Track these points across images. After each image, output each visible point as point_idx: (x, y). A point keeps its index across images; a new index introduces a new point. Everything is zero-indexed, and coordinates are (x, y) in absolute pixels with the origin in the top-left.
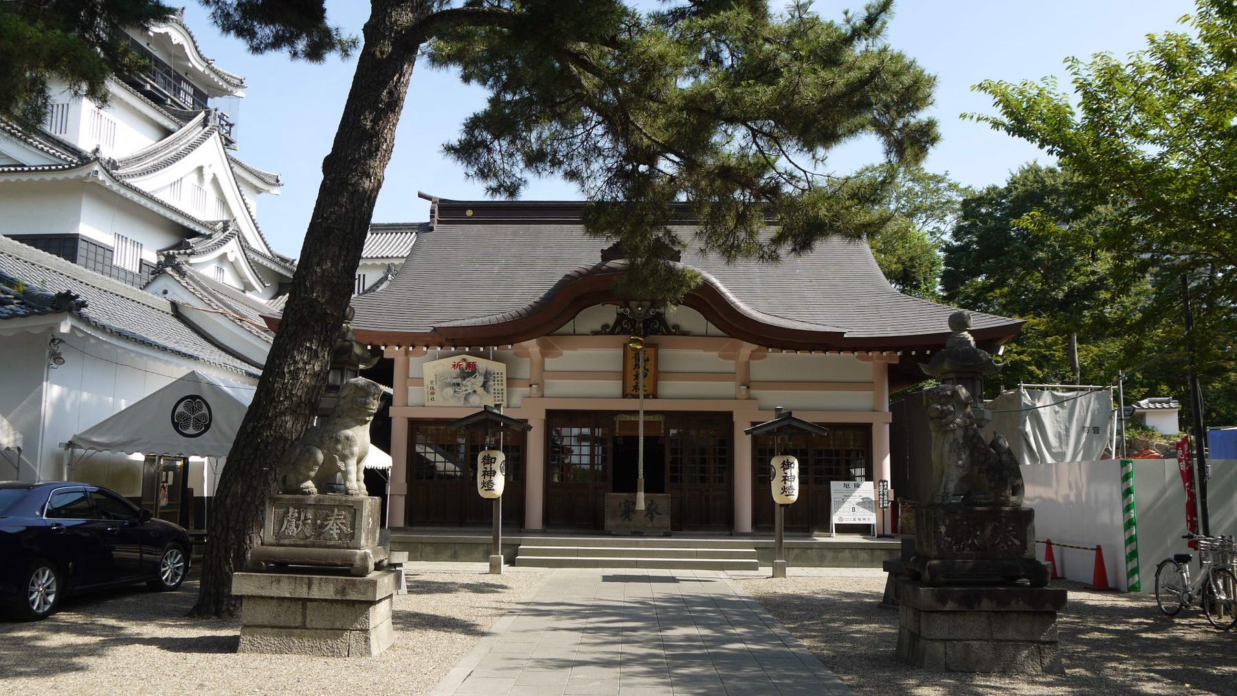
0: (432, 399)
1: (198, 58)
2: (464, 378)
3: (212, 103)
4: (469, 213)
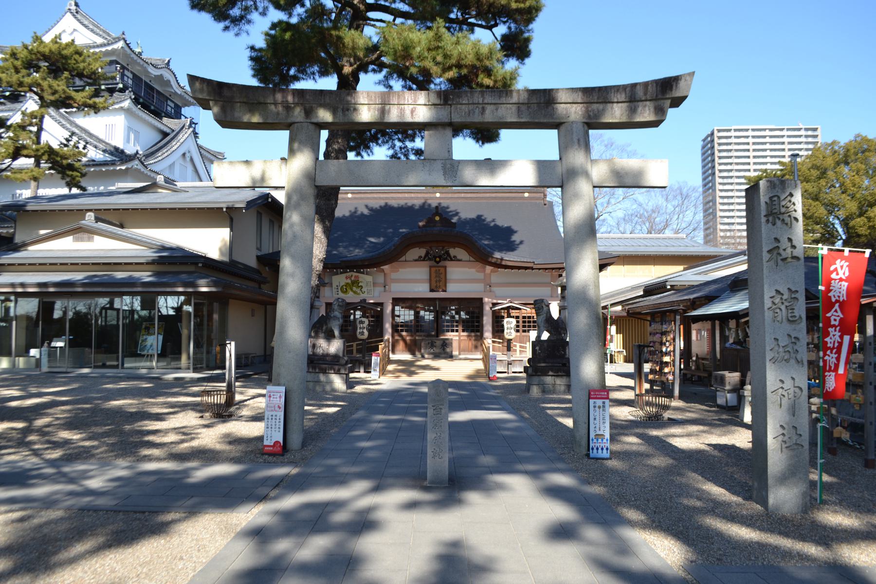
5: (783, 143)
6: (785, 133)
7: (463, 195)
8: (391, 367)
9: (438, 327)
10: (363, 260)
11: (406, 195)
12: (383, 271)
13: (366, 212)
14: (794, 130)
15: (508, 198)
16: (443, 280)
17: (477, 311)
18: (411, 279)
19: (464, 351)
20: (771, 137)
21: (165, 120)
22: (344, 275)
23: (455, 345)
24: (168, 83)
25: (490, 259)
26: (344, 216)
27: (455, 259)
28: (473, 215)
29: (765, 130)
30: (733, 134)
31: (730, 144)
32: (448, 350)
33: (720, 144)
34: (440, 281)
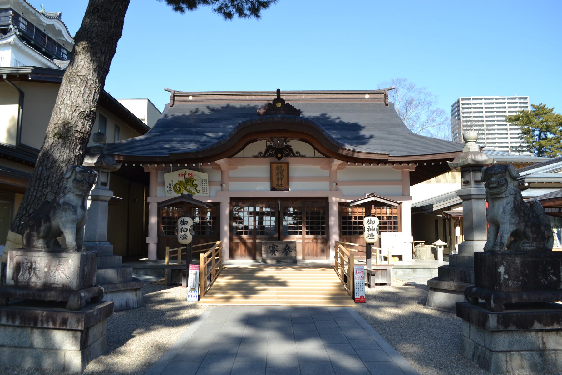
5: (505, 107)
6: (506, 101)
7: (304, 97)
8: (222, 281)
9: (280, 232)
10: (195, 152)
11: (247, 97)
12: (219, 168)
13: (207, 111)
14: (512, 98)
15: (349, 99)
16: (285, 177)
17: (321, 211)
18: (250, 177)
19: (309, 255)
20: (497, 103)
21: (56, 61)
22: (177, 173)
23: (299, 248)
24: (59, 33)
25: (340, 151)
26: (184, 115)
27: (298, 155)
28: (317, 114)
29: (493, 99)
30: (471, 101)
31: (470, 108)
32: (293, 254)
33: (463, 108)
34: (282, 179)
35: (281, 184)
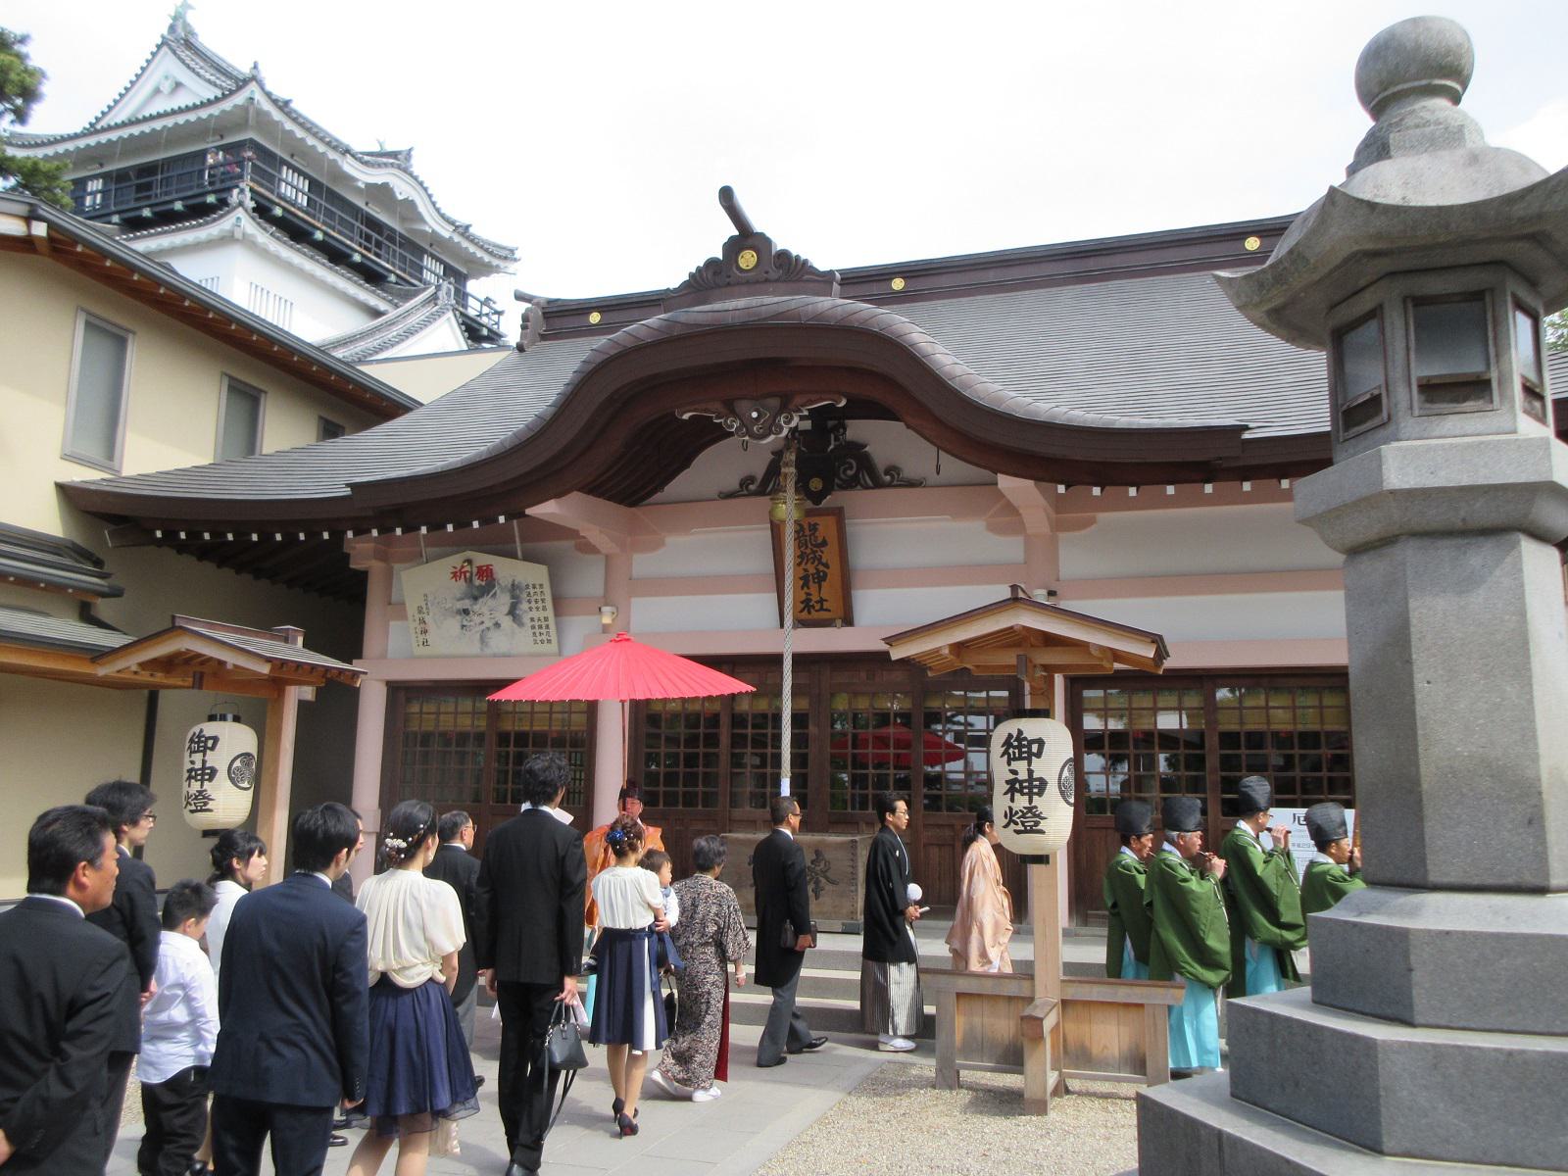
0: (425, 643)
1: (441, 221)
2: (476, 598)
3: (473, 286)
4: (595, 318)
16: (834, 572)
27: (893, 479)
34: (821, 578)
35: (821, 601)
